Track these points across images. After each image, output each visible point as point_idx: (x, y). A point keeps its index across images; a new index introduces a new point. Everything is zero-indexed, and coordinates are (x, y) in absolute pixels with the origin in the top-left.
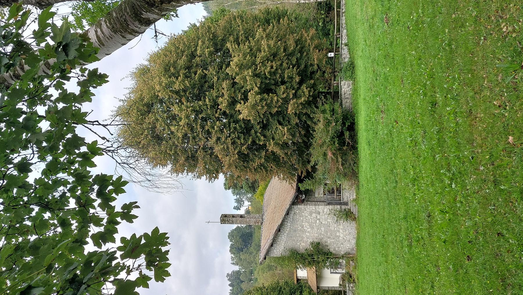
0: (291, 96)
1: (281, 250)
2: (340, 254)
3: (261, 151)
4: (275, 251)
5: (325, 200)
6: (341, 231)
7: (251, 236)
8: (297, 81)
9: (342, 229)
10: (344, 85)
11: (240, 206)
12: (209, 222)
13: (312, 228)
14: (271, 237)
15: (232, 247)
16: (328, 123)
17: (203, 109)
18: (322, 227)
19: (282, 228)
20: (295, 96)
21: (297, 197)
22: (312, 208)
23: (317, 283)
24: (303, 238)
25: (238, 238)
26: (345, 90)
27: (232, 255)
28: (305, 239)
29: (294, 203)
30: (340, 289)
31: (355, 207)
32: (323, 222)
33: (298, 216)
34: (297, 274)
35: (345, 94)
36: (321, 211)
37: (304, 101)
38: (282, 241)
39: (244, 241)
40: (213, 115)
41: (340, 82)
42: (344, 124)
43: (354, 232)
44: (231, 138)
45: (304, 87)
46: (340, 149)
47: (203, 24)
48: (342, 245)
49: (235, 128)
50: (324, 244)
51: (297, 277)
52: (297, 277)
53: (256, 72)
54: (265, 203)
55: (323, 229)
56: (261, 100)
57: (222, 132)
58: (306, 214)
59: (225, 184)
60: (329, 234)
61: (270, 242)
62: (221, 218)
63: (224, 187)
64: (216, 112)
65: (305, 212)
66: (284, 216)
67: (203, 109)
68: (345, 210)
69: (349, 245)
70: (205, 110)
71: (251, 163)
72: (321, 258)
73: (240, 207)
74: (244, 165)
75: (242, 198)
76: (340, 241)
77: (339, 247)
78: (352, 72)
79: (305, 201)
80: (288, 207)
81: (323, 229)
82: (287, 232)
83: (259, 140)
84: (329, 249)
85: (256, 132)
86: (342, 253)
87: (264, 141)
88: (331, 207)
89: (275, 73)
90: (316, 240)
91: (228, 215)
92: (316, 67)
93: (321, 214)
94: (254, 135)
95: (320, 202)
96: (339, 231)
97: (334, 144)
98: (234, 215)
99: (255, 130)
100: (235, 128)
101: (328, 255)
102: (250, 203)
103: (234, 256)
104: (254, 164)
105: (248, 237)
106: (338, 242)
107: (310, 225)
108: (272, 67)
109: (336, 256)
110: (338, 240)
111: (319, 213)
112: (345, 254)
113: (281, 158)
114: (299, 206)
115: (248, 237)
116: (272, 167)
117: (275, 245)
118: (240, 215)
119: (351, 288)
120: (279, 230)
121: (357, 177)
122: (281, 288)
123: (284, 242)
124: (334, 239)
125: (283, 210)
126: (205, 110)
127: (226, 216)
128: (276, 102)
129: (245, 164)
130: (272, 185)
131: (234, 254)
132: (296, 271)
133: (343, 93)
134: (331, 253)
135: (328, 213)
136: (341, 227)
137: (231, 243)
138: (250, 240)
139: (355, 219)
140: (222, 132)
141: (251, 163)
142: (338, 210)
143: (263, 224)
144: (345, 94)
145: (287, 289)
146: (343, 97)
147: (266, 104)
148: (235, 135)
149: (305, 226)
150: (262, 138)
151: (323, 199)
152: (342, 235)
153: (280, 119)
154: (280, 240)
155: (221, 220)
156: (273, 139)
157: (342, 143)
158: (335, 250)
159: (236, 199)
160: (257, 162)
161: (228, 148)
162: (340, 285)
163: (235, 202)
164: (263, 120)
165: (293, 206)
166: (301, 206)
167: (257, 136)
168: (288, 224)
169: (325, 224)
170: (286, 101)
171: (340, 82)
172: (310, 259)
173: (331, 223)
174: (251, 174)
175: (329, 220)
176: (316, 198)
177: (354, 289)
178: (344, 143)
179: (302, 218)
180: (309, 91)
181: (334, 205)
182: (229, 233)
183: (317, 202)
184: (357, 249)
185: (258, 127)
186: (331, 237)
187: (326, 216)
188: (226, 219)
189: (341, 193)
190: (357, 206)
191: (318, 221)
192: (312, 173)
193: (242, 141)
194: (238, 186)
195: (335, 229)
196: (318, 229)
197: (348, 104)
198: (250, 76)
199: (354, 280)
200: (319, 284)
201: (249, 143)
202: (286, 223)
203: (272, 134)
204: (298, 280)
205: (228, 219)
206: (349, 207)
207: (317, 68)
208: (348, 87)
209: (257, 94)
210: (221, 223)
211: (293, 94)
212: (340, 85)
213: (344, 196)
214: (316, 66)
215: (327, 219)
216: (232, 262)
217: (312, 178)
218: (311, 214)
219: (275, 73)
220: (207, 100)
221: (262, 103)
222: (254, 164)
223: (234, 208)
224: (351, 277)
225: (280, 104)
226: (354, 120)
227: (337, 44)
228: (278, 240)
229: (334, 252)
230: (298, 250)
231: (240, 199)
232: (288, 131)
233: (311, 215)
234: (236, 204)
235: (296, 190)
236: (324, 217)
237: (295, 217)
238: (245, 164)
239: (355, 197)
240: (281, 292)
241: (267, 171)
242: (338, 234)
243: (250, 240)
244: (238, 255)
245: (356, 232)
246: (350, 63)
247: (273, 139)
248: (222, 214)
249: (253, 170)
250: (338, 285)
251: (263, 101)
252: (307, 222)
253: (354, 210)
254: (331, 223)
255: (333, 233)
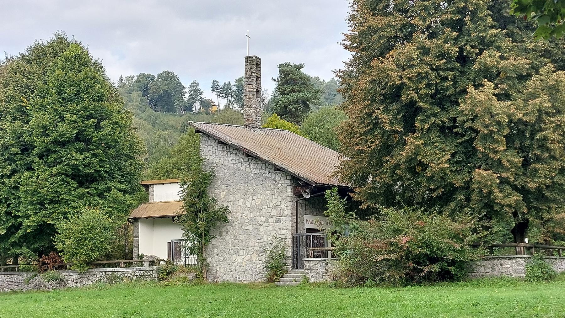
0: (504, 175)
1: (212, 158)
3: (403, 123)
4: (210, 148)
5: (299, 232)
6: (248, 257)
7: (168, 110)
8: (529, 185)
10: (518, 264)
11: (219, 92)
12: (248, 37)
13: (252, 210)
14: (236, 142)
15: (149, 78)
16: (456, 237)
17: (479, 25)
18: (254, 226)
19: (250, 160)
20: (504, 181)
21: (307, 184)
23: (145, 217)
24: (234, 194)
25: (165, 88)
26: (509, 266)
27: (135, 78)
28: (232, 198)
29: (296, 180)
30: (135, 256)
32: (262, 228)
34: (158, 185)
35: (501, 265)
36: (281, 225)
37: (495, 198)
38: (227, 159)
39: (160, 97)
40: (467, 41)
41: (523, 258)
42: (453, 263)
43: (247, 279)
44: (429, 72)
45: (517, 197)
46: (407, 257)
47: (50, 45)
48: (222, 259)
49: (446, 79)
50: (223, 230)
51: (154, 184)
52: (154, 184)
53: (544, 115)
55: (250, 227)
56: (499, 123)
57: (438, 57)
58: (277, 199)
59: (288, 65)
60: (242, 237)
61: (227, 139)
62: (255, 57)
63: (283, 63)
64: (472, 47)
65: (280, 198)
66: (274, 163)
67: (479, 25)
68: (285, 264)
69: (222, 270)
70: (477, 27)
71: (381, 107)
72: (202, 224)
74: (378, 95)
78: (540, 277)
80: (290, 170)
81: (250, 227)
82: (243, 168)
83: (422, 121)
84: (214, 237)
85: (435, 115)
86: (209, 260)
87: (422, 129)
88: (289, 241)
89: (542, 147)
90: (230, 216)
92: (546, 216)
93: (276, 224)
94: (431, 112)
95: (297, 223)
96: (247, 254)
97: (419, 247)
98: (259, 79)
99: (438, 113)
100: (446, 79)
101: (205, 236)
102: (222, 107)
103: (134, 80)
104: (380, 111)
105: (167, 104)
107: (256, 206)
108: (553, 142)
109: (204, 250)
111: (278, 221)
112: (208, 265)
113: (388, 158)
114: (289, 188)
115: (167, 104)
116: (372, 142)
117: (220, 148)
118: (259, 89)
119: (150, 274)
120: (248, 155)
121: (354, 285)
122: (131, 158)
123: (225, 162)
124: (234, 246)
125: (281, 161)
126: (477, 27)
127: (258, 65)
128: (494, 148)
129: (379, 97)
130: (307, 144)
131: (138, 81)
133: (502, 262)
134: (209, 241)
135: (279, 236)
136: (254, 258)
137: (156, 76)
138: (162, 108)
139: (271, 280)
140: (438, 57)
141: (381, 107)
142: (285, 252)
144: (501, 265)
145: (131, 169)
146: (495, 261)
147: (492, 132)
148: (433, 80)
149: (255, 197)
150: (427, 126)
151: (300, 227)
152: (239, 258)
153: (458, 156)
154: (229, 155)
155: (252, 57)
156: (425, 145)
157: (419, 260)
159: (229, 84)
160: (385, 118)
161: (411, 66)
162: (142, 256)
163: (225, 83)
164: (457, 127)
165: (289, 178)
167: (428, 117)
168: (257, 170)
169: (259, 230)
170: (497, 165)
171: (523, 258)
172: (200, 205)
173: (261, 241)
174: (362, 106)
175: (265, 238)
177: (148, 279)
178: (419, 264)
180: (510, 206)
181: (293, 247)
182: (172, 73)
183: (297, 218)
184: (216, 284)
185: (445, 119)
187: (274, 233)
189: (314, 257)
190: (294, 284)
192: (356, 211)
193: (423, 92)
194: (285, 86)
195: (251, 248)
197: (482, 269)
198: (541, 104)
199: (163, 278)
200: (143, 222)
201: (421, 104)
202: (260, 166)
203: (433, 143)
204: (147, 187)
205: (254, 69)
207: (545, 218)
208: (514, 271)
209: (509, 116)
210: (246, 58)
211: (507, 178)
212: (518, 258)
214: (549, 216)
215: (268, 235)
216: (124, 78)
217: (347, 210)
219: (542, 147)
220: (494, 31)
221: (493, 126)
222: (380, 111)
223: (215, 81)
224: (168, 274)
225: (492, 155)
226: (458, 280)
227: (211, 239)
229: (210, 246)
231: (230, 91)
232: (441, 169)
233: (275, 208)
234: (221, 84)
235: (319, 183)
236: (271, 229)
237: (270, 182)
238: (379, 97)
239: (313, 280)
240: (126, 158)
241: (365, 133)
242: (242, 252)
243: (162, 108)
244: (136, 88)
245: (247, 283)
246: (553, 273)
247: (425, 145)
249: (368, 111)
250: (141, 253)
251: (498, 127)
253: (287, 279)
254: (261, 241)
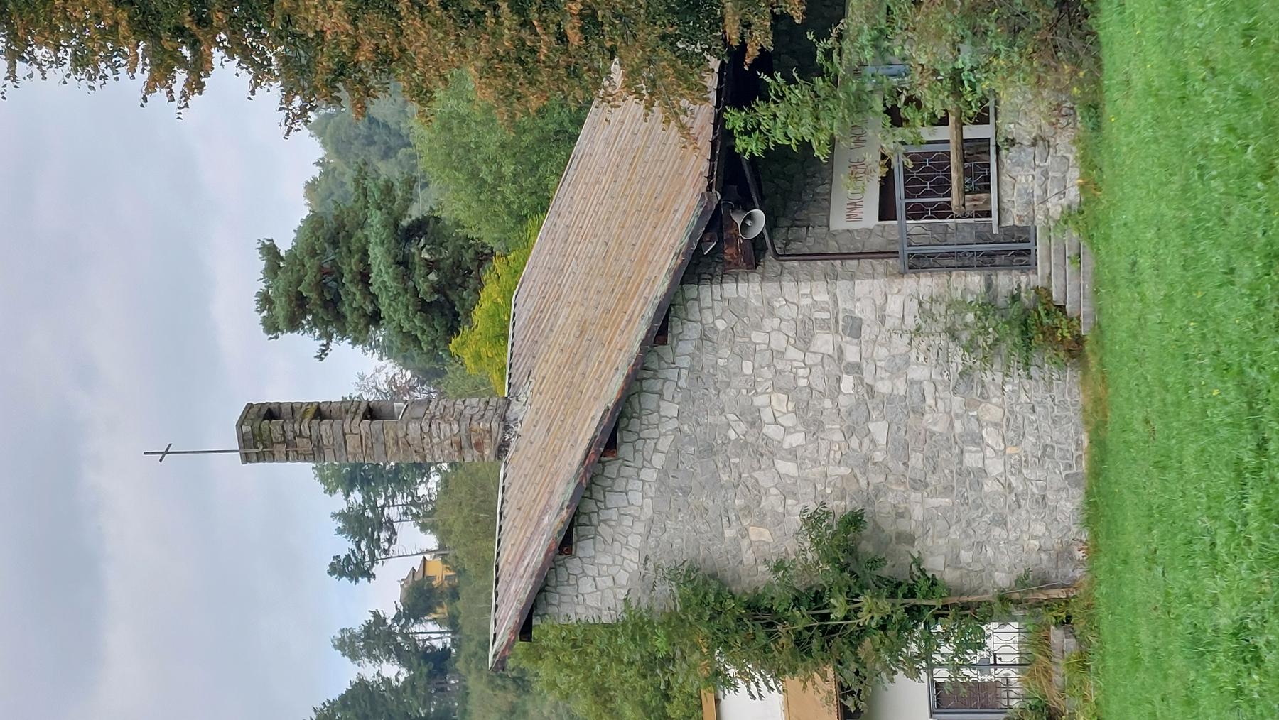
1: (623, 578)
2: (988, 585)
4: (586, 586)
6: (990, 436)
9: (996, 425)
11: (372, 554)
13: (814, 426)
14: (563, 491)
18: (874, 414)
22: (810, 295)
24: (757, 493)
28: (772, 501)
31: (1074, 267)
32: (883, 387)
33: (726, 352)
38: (627, 521)
48: (997, 532)
50: (889, 528)
54: (518, 337)
55: (879, 430)
59: (265, 301)
60: (916, 460)
61: (553, 523)
65: (768, 324)
66: (636, 348)
68: (1015, 298)
69: (1039, 529)
73: (374, 560)
75: (380, 502)
76: (988, 503)
77: (980, 545)
79: (769, 261)
80: (661, 286)
81: (879, 430)
82: (658, 460)
84: (918, 562)
86: (1002, 579)
88: (927, 284)
90: (840, 507)
91: (286, 411)
93: (866, 333)
96: (978, 441)
98: (324, 408)
106: (975, 514)
107: (801, 411)
109: (965, 599)
110: (972, 496)
112: (1022, 582)
114: (730, 288)
117: (584, 548)
123: (640, 527)
124: (948, 490)
127: (271, 413)
130: (561, 224)
132: (717, 701)
134: (934, 583)
135: (910, 323)
136: (993, 412)
139: (1075, 350)
142: (969, 298)
143: (511, 451)
149: (767, 416)
151: (876, 243)
152: (995, 467)
154: (613, 514)
158: (954, 562)
159: (343, 516)
163: (340, 531)
165: (692, 291)
166: (742, 286)
169: (890, 398)
173: (928, 389)
174: (418, 23)
175: (917, 373)
176: (834, 235)
179: (748, 368)
184: (1093, 550)
186: (932, 479)
187: (900, 343)
188: (275, 427)
189: (987, 189)
190: (1088, 262)
191: (848, 382)
196: (849, 432)
202: (649, 401)
205: (288, 428)
206: (1037, 280)
213: (1006, 189)
218: (803, 337)
228: (604, 514)
229: (950, 576)
230: (729, 574)
231: (369, 513)
233: (804, 341)
234: (344, 546)
236: (883, 352)
237: (707, 359)
239: (1073, 194)
242: (972, 459)
248: (250, 406)
252: (781, 390)
254: (928, 389)
255: (944, 454)
